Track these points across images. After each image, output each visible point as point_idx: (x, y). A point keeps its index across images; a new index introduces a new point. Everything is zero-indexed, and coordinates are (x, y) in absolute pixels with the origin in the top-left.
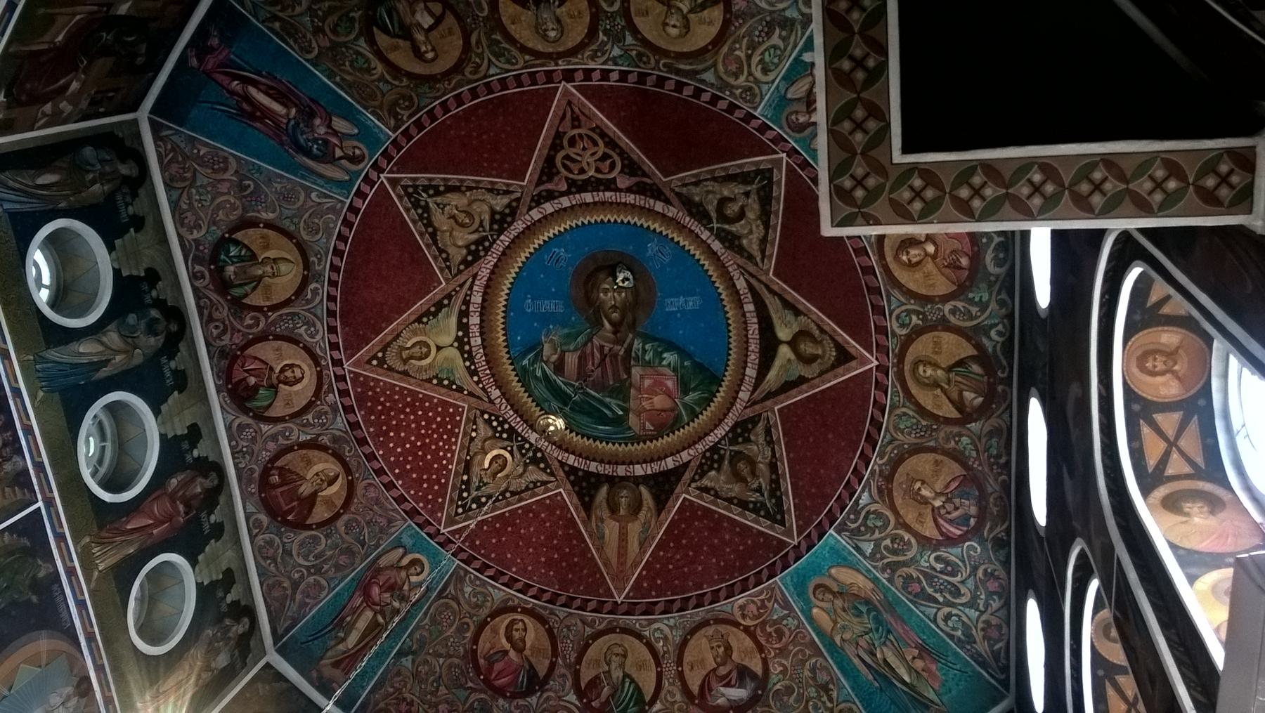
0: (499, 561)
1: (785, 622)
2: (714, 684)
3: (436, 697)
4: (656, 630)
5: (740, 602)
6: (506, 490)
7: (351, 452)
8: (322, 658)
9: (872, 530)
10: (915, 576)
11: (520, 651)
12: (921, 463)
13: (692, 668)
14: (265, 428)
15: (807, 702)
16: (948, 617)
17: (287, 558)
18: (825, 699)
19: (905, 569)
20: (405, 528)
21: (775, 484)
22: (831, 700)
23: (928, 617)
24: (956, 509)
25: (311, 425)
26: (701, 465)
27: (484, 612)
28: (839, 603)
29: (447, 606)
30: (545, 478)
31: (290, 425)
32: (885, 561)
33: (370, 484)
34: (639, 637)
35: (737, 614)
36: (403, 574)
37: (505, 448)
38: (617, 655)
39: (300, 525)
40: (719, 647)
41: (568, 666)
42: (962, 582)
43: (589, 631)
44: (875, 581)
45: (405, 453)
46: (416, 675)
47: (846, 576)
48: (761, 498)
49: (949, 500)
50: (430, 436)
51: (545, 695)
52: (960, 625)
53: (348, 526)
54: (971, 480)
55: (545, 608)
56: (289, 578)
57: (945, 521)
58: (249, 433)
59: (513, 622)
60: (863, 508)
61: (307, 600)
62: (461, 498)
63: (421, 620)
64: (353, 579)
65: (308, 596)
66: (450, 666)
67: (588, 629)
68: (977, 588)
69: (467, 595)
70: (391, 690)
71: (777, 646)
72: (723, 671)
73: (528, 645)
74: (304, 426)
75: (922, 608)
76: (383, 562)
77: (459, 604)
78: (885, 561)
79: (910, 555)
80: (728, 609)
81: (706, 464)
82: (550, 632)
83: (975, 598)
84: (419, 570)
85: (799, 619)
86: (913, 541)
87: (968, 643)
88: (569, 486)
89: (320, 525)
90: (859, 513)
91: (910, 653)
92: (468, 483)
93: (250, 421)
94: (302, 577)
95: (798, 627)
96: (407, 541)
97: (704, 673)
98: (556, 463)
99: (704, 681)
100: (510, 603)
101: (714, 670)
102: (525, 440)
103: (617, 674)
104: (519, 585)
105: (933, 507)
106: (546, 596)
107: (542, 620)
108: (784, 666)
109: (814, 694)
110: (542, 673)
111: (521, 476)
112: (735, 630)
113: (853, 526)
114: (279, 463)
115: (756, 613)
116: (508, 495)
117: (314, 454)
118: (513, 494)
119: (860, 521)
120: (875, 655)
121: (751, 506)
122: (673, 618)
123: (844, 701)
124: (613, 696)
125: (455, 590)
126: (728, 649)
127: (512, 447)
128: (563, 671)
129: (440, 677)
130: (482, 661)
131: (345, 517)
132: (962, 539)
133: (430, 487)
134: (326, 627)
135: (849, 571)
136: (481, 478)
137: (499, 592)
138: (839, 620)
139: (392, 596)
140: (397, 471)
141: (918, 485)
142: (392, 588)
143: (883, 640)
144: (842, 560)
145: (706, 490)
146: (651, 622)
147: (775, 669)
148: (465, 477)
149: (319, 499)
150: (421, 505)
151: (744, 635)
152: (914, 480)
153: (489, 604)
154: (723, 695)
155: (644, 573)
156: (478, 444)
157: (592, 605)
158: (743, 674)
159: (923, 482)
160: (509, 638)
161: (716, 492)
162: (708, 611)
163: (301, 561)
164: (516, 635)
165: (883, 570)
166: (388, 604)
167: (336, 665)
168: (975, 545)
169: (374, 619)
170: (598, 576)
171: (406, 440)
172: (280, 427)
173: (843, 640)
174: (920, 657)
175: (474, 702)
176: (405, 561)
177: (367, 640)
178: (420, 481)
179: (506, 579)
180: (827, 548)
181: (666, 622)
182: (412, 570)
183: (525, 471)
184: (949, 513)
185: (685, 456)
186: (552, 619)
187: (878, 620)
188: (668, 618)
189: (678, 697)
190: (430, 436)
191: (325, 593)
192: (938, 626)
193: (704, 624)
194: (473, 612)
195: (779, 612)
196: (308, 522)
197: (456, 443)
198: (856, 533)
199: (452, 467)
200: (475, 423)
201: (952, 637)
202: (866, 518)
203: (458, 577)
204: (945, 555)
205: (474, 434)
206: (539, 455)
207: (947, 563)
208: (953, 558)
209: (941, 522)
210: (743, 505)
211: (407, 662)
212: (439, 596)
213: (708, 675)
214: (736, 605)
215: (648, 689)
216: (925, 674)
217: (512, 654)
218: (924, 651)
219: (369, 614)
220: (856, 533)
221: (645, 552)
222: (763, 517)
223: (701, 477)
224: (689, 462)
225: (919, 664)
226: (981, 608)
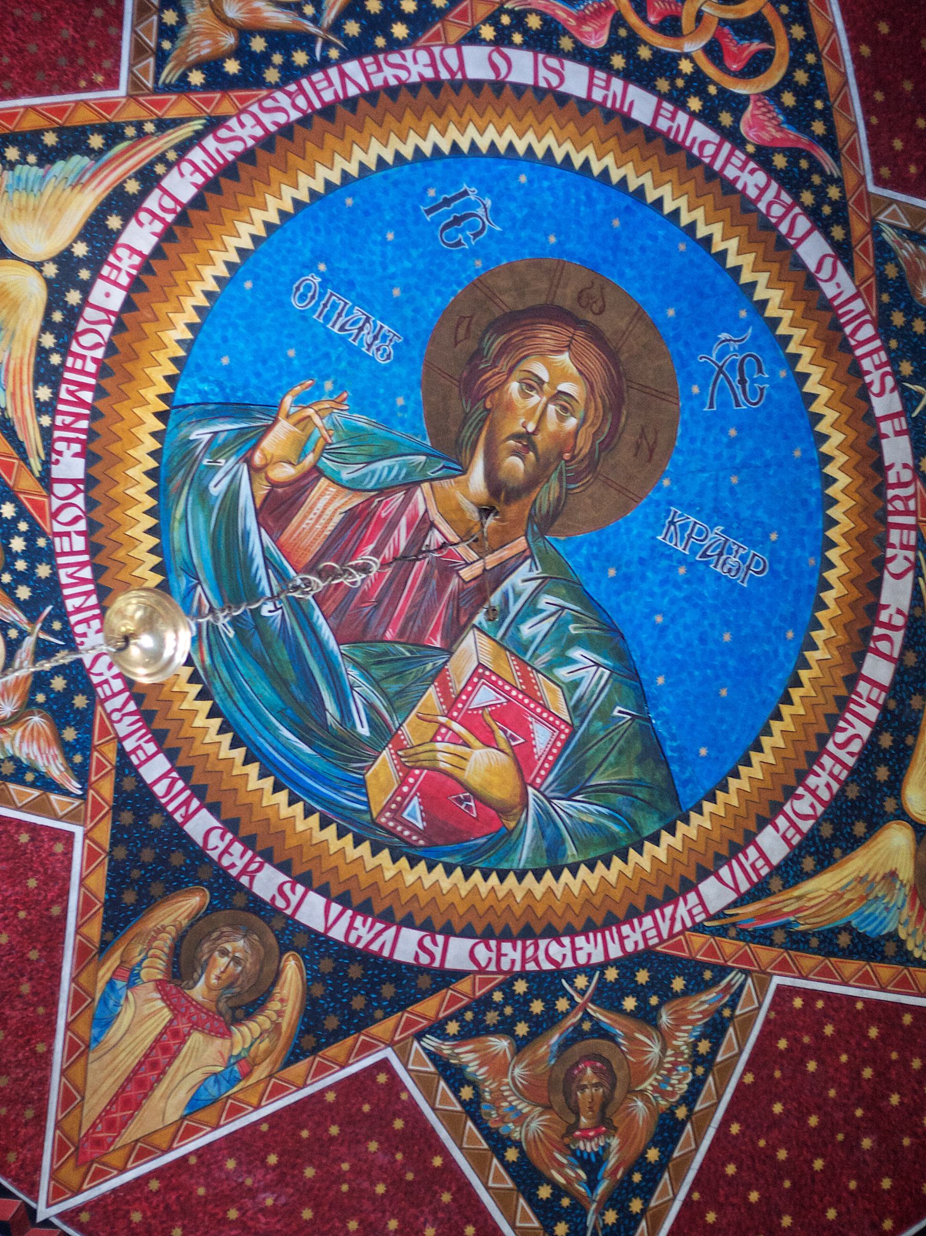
26: (485, 1003)
30: (56, 769)
81: (499, 1007)
88: (104, 834)
121: (544, 1192)
155: (154, 1185)
161: (478, 1095)
170: (29, 1114)
206: (80, 701)
221: (190, 1132)
223: (464, 1036)
224: (460, 975)
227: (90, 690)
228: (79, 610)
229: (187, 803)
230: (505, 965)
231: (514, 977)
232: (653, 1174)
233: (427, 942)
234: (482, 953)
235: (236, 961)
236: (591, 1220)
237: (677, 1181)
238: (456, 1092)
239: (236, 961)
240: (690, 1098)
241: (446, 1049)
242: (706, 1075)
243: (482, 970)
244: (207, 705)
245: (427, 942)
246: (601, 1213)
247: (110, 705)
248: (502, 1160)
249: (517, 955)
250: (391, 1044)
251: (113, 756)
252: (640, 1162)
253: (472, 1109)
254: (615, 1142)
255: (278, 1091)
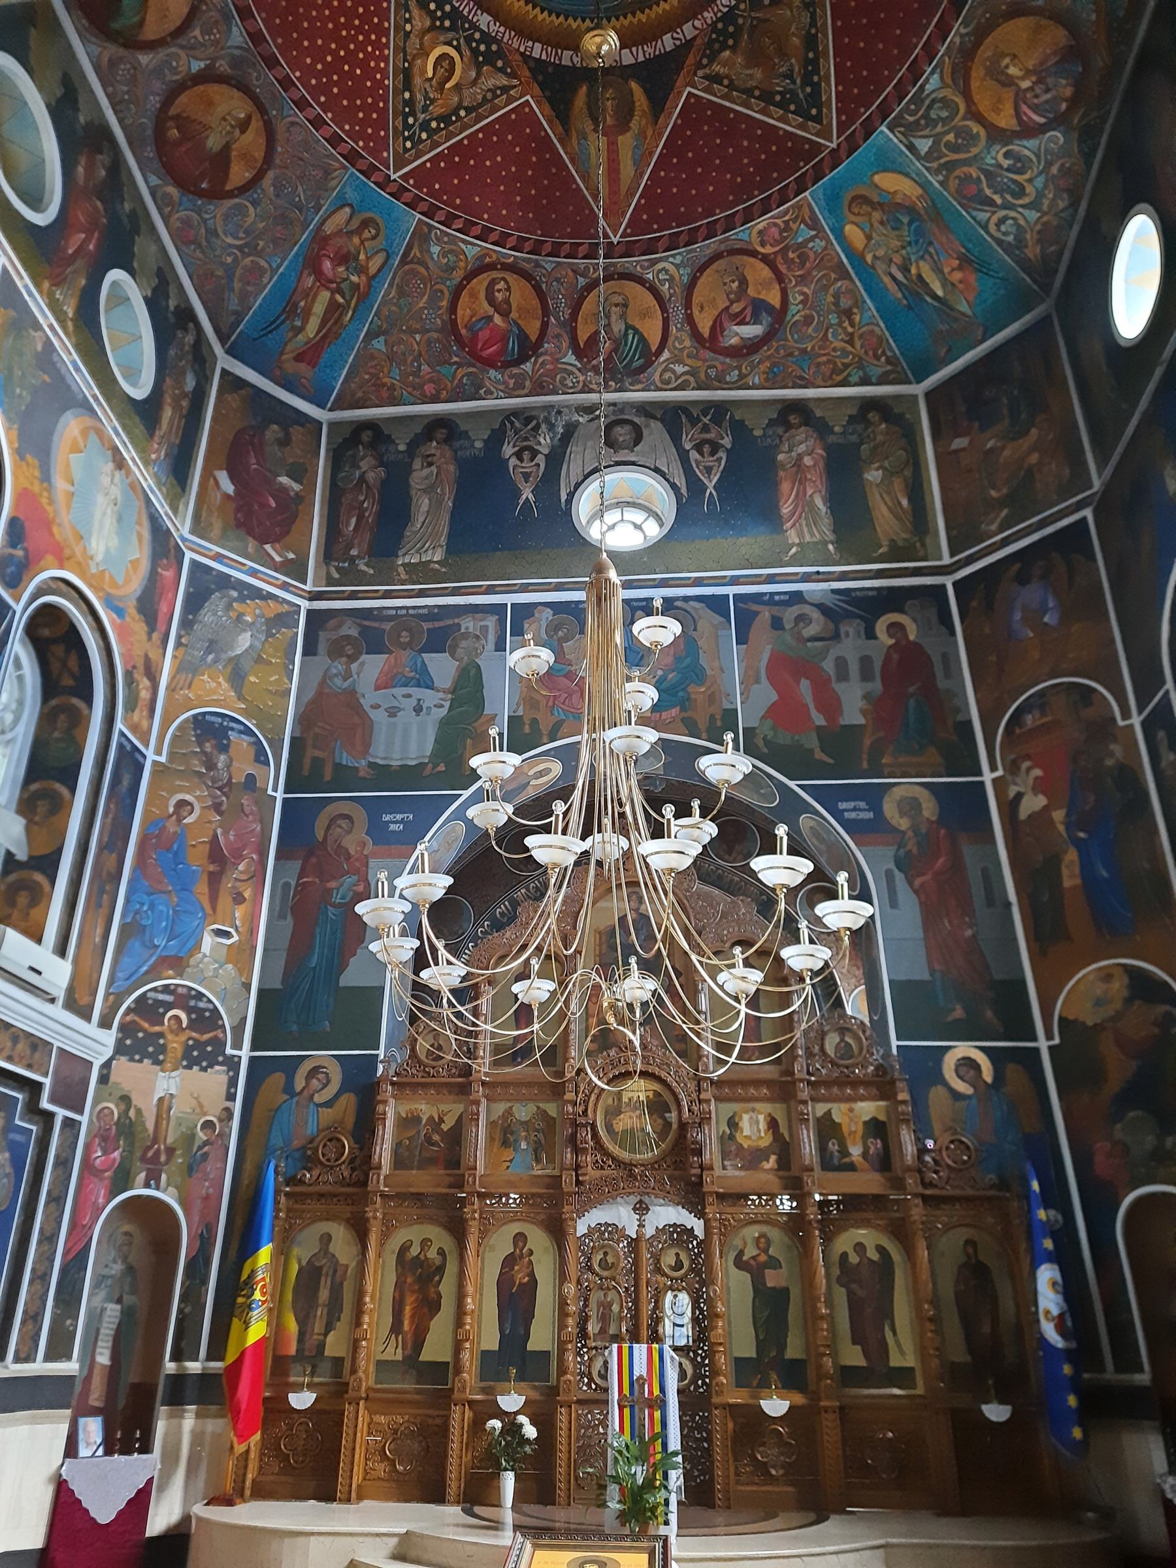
0: (465, 208)
1: (811, 245)
2: (726, 324)
3: (418, 377)
4: (660, 271)
5: (760, 226)
6: (460, 106)
7: (263, 79)
8: (282, 354)
9: (931, 123)
10: (974, 175)
11: (505, 314)
12: (1017, 30)
13: (702, 308)
14: (144, 59)
15: (827, 330)
16: (1002, 221)
17: (214, 240)
18: (846, 324)
19: (965, 169)
20: (348, 180)
21: (812, 67)
22: (852, 325)
23: (979, 223)
24: (1048, 90)
25: (203, 45)
26: (711, 42)
27: (458, 275)
28: (877, 215)
29: (414, 273)
30: (504, 81)
31: (173, 50)
32: (942, 161)
33: (293, 124)
34: (641, 281)
35: (756, 240)
36: (356, 240)
37: (449, 44)
38: (617, 305)
39: (217, 193)
40: (733, 281)
41: (562, 325)
42: (1030, 181)
43: (582, 281)
44: (924, 185)
45: (329, 69)
46: (391, 358)
47: (889, 182)
48: (792, 86)
49: (1040, 81)
50: (354, 39)
51: (541, 360)
52: (1014, 230)
53: (278, 186)
54: (1074, 53)
55: (528, 261)
56: (222, 264)
57: (1030, 107)
58: (123, 68)
59: (493, 282)
60: (928, 95)
61: (249, 288)
62: (407, 126)
63: (387, 293)
64: (297, 253)
65: (248, 283)
66: (429, 342)
67: (581, 280)
68: (1046, 186)
69: (435, 257)
70: (367, 377)
71: (798, 273)
72: (736, 308)
73: (514, 307)
74: (193, 48)
75: (975, 213)
76: (329, 228)
77: (427, 268)
78: (942, 161)
79: (974, 151)
80: (745, 236)
81: (716, 40)
82: (537, 288)
83: (1040, 195)
84: (373, 232)
85: (828, 241)
86: (983, 133)
87: (1018, 248)
88: (537, 90)
89: (243, 190)
90: (923, 101)
91: (949, 264)
92: (410, 103)
93: (122, 52)
94: (236, 260)
95: (825, 248)
96: (351, 195)
97: (716, 313)
98: (518, 57)
99: (715, 322)
100: (488, 260)
101: (727, 308)
102: (475, 27)
103: (618, 327)
104: (494, 237)
105: (1019, 88)
106: (528, 246)
107: (526, 276)
108: (804, 294)
109: (834, 321)
110: (533, 338)
111: (474, 82)
112: (752, 260)
113: (911, 119)
114: (173, 111)
115: (777, 236)
116: (462, 113)
117: (215, 90)
118: (469, 110)
119: (921, 113)
120: (909, 271)
121: (778, 98)
122: (678, 255)
123: (868, 324)
124: (616, 350)
125: (421, 252)
126: (744, 283)
127: (458, 40)
128: (557, 330)
129: (420, 355)
130: (463, 332)
131: (271, 174)
132: (1043, 129)
133: (368, 116)
134: (278, 318)
135: (895, 176)
136: (427, 92)
137: (473, 249)
138: (874, 235)
139: (347, 269)
140: (323, 99)
141: (1007, 60)
142: (344, 258)
143: (921, 253)
144: (888, 164)
145: (716, 79)
146: (654, 262)
147: (795, 298)
148: (407, 95)
149: (234, 153)
150: (361, 143)
151: (762, 265)
152: (1003, 55)
153: (462, 264)
154: (737, 334)
155: (643, 201)
156: (414, 41)
157: (582, 250)
158: (758, 308)
159: (1015, 56)
160: (491, 300)
161: (731, 81)
162: (721, 242)
163: (229, 240)
164: (499, 296)
165: (937, 171)
166: (345, 280)
167: (299, 358)
168: (1059, 135)
169: (332, 299)
170: (587, 212)
171: (325, 50)
172: (162, 53)
173: (875, 257)
174: (960, 268)
175: (463, 377)
176: (355, 224)
177: (328, 326)
178: (353, 109)
179: (477, 230)
180: (874, 150)
181: (671, 259)
182: (366, 234)
183: (479, 74)
184: (1036, 96)
185: (688, 30)
186: (537, 274)
187: (919, 233)
188: (673, 256)
189: (687, 343)
190: (354, 39)
191: (268, 275)
192: (988, 232)
193: (716, 257)
194: (446, 275)
195: (805, 233)
196: (228, 188)
197: (387, 46)
198: (911, 130)
199: (389, 82)
200: (408, 10)
201: (1000, 242)
202: (930, 107)
203: (421, 236)
204: (1016, 148)
205: (408, 27)
206: (494, 47)
207: (1018, 158)
208: (1027, 152)
209: (1024, 108)
210: (767, 97)
211: (379, 344)
212: (403, 261)
213: (720, 315)
214: (755, 231)
215: (654, 341)
216: (961, 286)
217: (497, 319)
218: (965, 262)
219: (325, 295)
220: (911, 130)
221: (642, 175)
222: (793, 113)
223: (711, 62)
224: (695, 38)
225: (957, 276)
226: (1045, 208)
227: (495, 40)
228: (470, 12)
229: (557, 53)
230: (709, 21)
231: (714, 23)
232: (815, 62)
233: (675, 35)
234: (697, 23)
235: (613, 99)
236: (801, 96)
237: (827, 60)
238: (721, 84)
239: (613, 99)
240: (813, 23)
241: (708, 71)
242: (815, 11)
243: (701, 30)
244: (538, 9)
245: (675, 35)
246: (803, 91)
247: (505, 40)
248: (755, 98)
249: (712, 14)
250: (688, 85)
251: (519, 58)
252: (808, 62)
253: (731, 86)
254: (793, 61)
255: (661, 135)
